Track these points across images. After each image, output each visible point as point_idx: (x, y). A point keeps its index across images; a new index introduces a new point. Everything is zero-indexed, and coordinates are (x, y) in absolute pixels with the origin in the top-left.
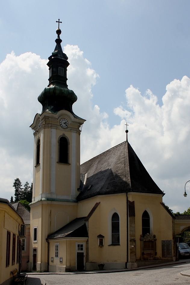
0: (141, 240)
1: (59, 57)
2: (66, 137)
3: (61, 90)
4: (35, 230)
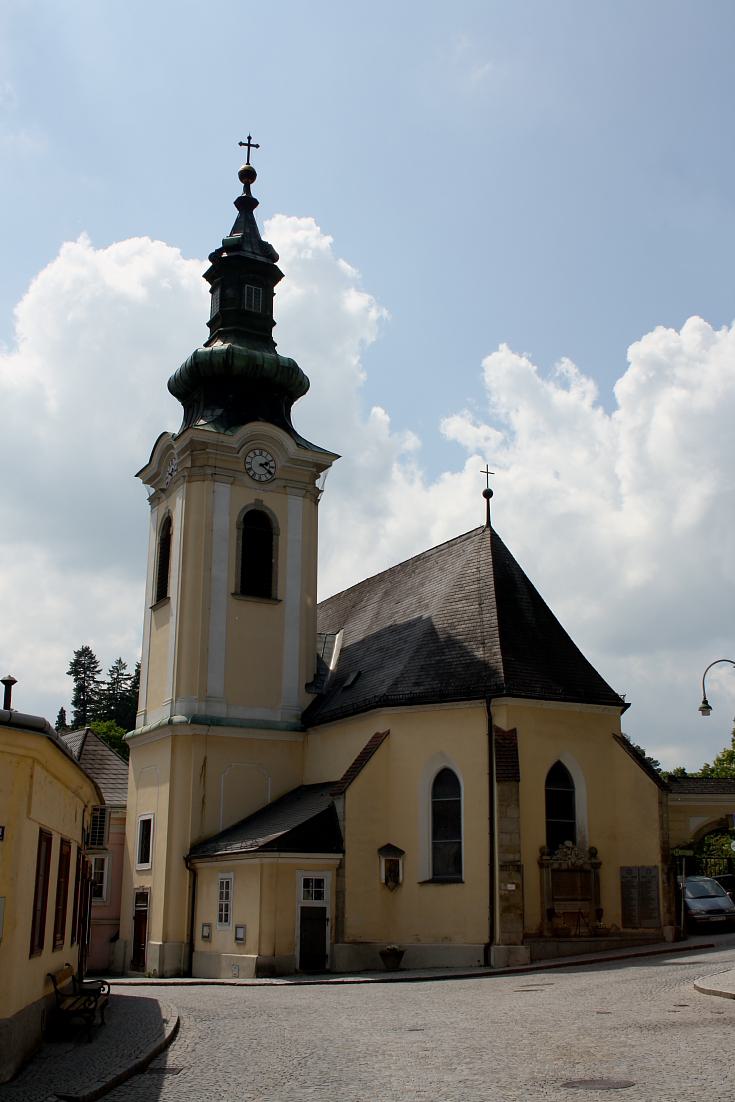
0: (541, 865)
1: (248, 252)
2: (267, 512)
3: (251, 359)
4: (146, 825)
